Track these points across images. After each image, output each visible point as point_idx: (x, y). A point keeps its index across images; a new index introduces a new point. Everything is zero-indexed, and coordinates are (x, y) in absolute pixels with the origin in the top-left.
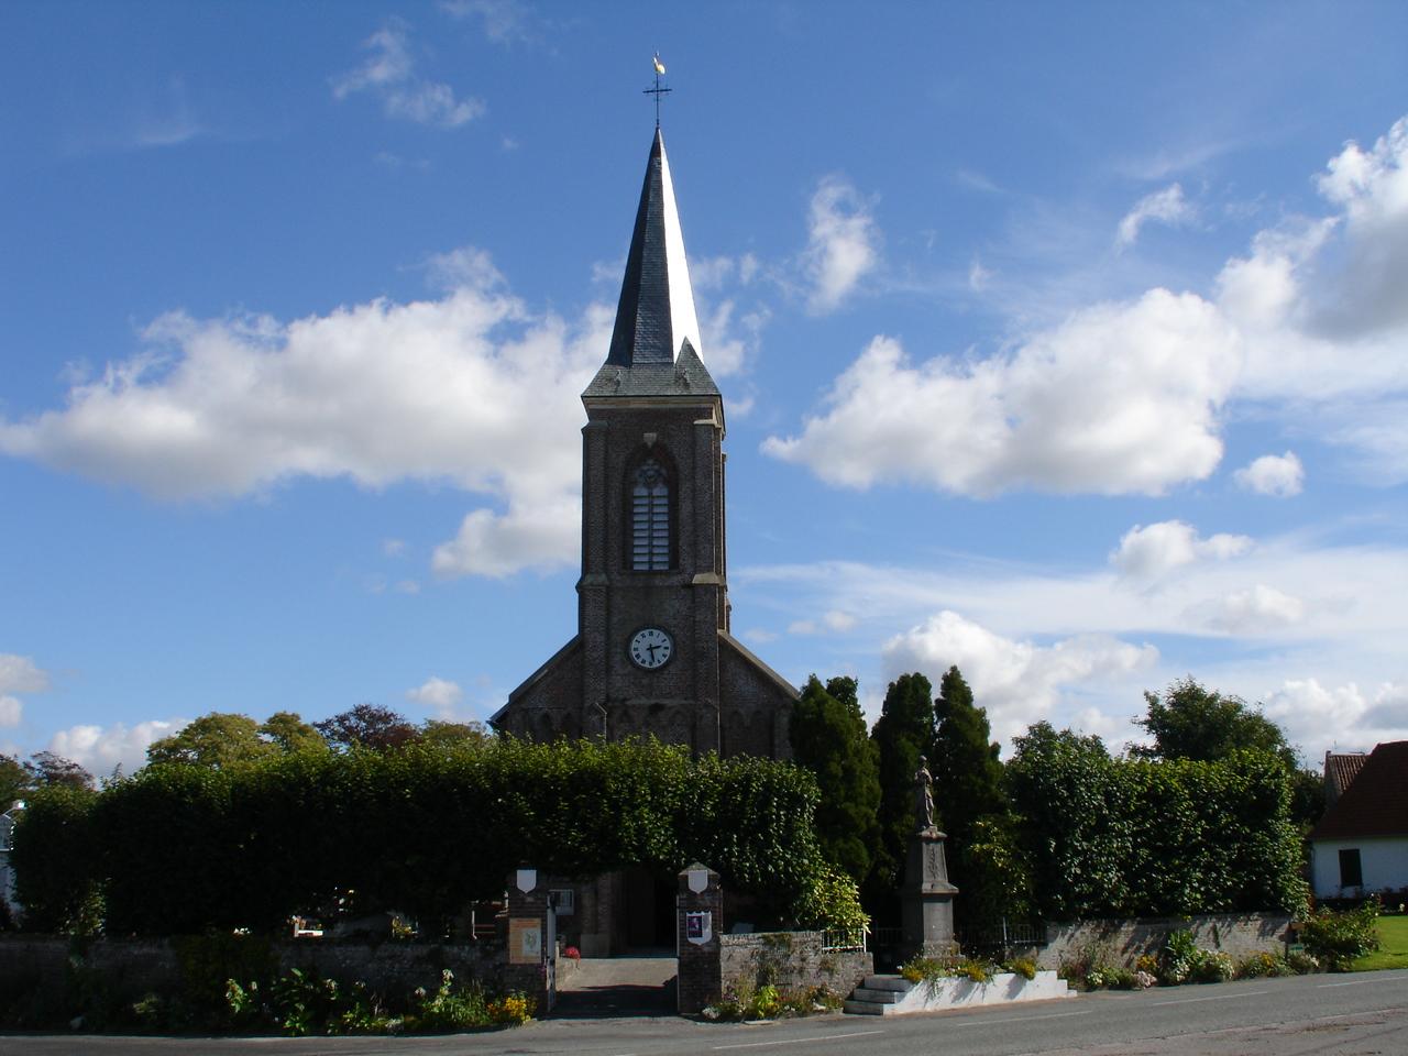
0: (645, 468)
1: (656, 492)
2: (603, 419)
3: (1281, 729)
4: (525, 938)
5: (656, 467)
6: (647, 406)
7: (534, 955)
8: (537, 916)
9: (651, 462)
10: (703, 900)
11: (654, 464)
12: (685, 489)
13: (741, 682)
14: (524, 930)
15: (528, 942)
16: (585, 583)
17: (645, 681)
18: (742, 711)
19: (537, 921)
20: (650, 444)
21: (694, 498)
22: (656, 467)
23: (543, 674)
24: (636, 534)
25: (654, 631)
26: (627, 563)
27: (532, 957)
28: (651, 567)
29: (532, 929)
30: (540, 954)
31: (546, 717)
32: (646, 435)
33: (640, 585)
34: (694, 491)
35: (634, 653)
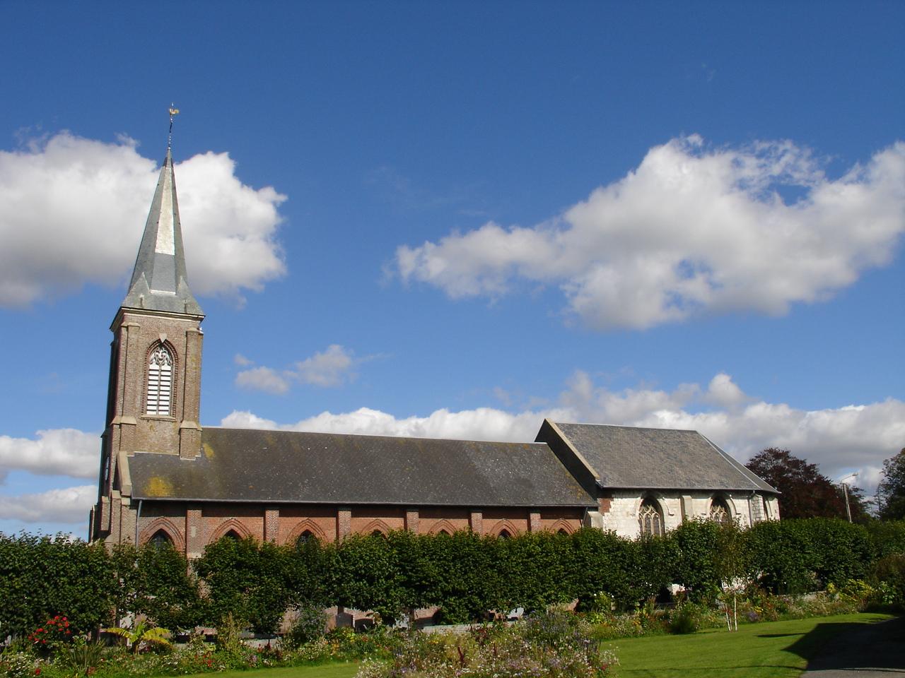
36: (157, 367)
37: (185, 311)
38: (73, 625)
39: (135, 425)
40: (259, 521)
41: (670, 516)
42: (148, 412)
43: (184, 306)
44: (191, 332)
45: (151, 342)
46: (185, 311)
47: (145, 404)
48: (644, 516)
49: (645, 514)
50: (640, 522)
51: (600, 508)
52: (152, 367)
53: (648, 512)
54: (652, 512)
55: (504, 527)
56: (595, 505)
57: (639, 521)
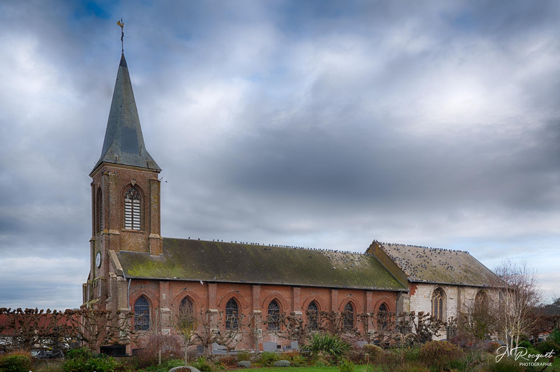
36: (130, 201)
37: (148, 166)
38: (119, 339)
39: (119, 235)
40: (164, 315)
41: (451, 300)
42: (126, 228)
43: (146, 163)
44: (152, 180)
45: (125, 185)
46: (148, 166)
47: (124, 211)
48: (434, 299)
49: (435, 297)
50: (432, 301)
51: (409, 293)
52: (127, 200)
53: (437, 296)
54: (439, 297)
55: (351, 300)
56: (406, 290)
57: (431, 300)
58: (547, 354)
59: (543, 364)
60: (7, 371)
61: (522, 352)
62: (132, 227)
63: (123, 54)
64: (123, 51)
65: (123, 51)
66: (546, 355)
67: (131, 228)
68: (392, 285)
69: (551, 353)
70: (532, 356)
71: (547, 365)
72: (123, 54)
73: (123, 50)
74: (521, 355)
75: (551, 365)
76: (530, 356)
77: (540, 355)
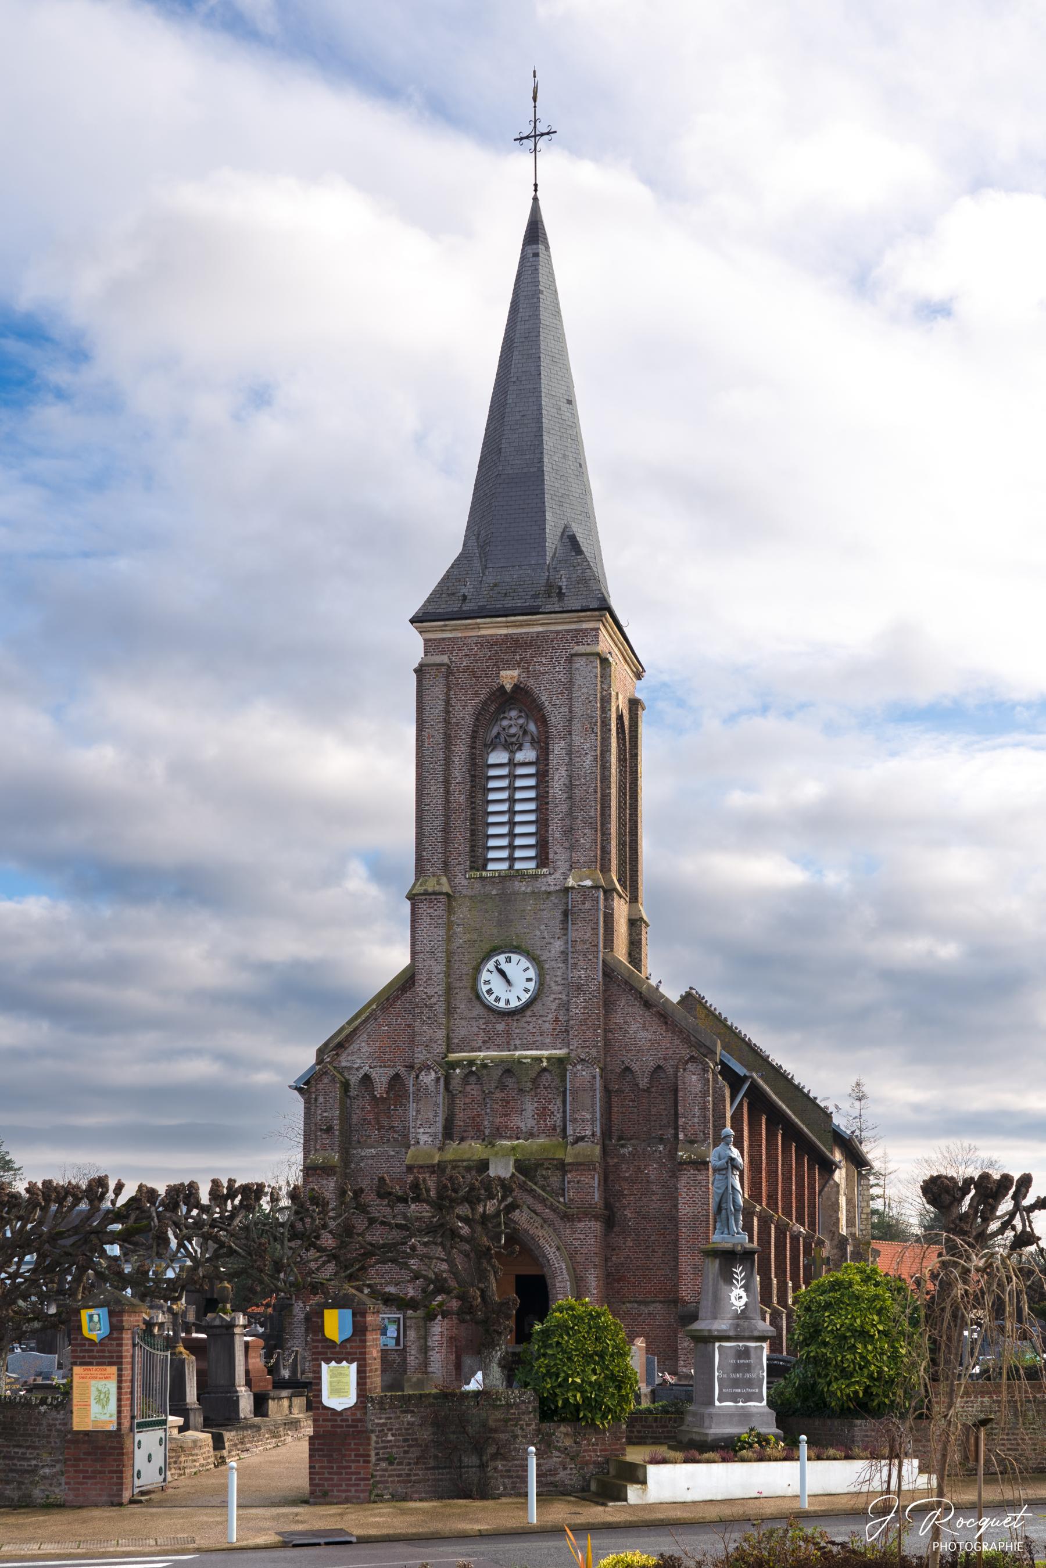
0: (505, 723)
1: (520, 757)
2: (442, 653)
3: (831, 1109)
4: (94, 1394)
5: (521, 721)
6: (504, 631)
7: (106, 1418)
8: (111, 1364)
9: (514, 714)
10: (893, 1308)
11: (520, 717)
12: (558, 749)
13: (634, 1027)
14: (93, 1382)
15: (99, 1401)
16: (615, 895)
17: (500, 1027)
18: (635, 1067)
19: (114, 1369)
20: (508, 687)
21: (570, 764)
22: (521, 721)
23: (359, 1020)
24: (492, 819)
25: (512, 956)
26: (478, 862)
27: (105, 1422)
28: (511, 867)
29: (104, 1382)
30: (115, 1418)
31: (367, 1078)
32: (503, 673)
33: (494, 892)
34: (570, 753)
35: (484, 988)
58: (1010, 1518)
59: (997, 1545)
60: (784, 1567)
61: (938, 1513)
62: (512, 859)
63: (535, 199)
64: (536, 190)
65: (536, 190)
66: (1006, 1521)
67: (504, 866)
68: (410, 1241)
69: (1021, 1514)
70: (968, 1523)
71: (1009, 1548)
72: (535, 199)
73: (536, 185)
74: (936, 1520)
75: (1020, 1548)
76: (963, 1522)
77: (991, 1520)
